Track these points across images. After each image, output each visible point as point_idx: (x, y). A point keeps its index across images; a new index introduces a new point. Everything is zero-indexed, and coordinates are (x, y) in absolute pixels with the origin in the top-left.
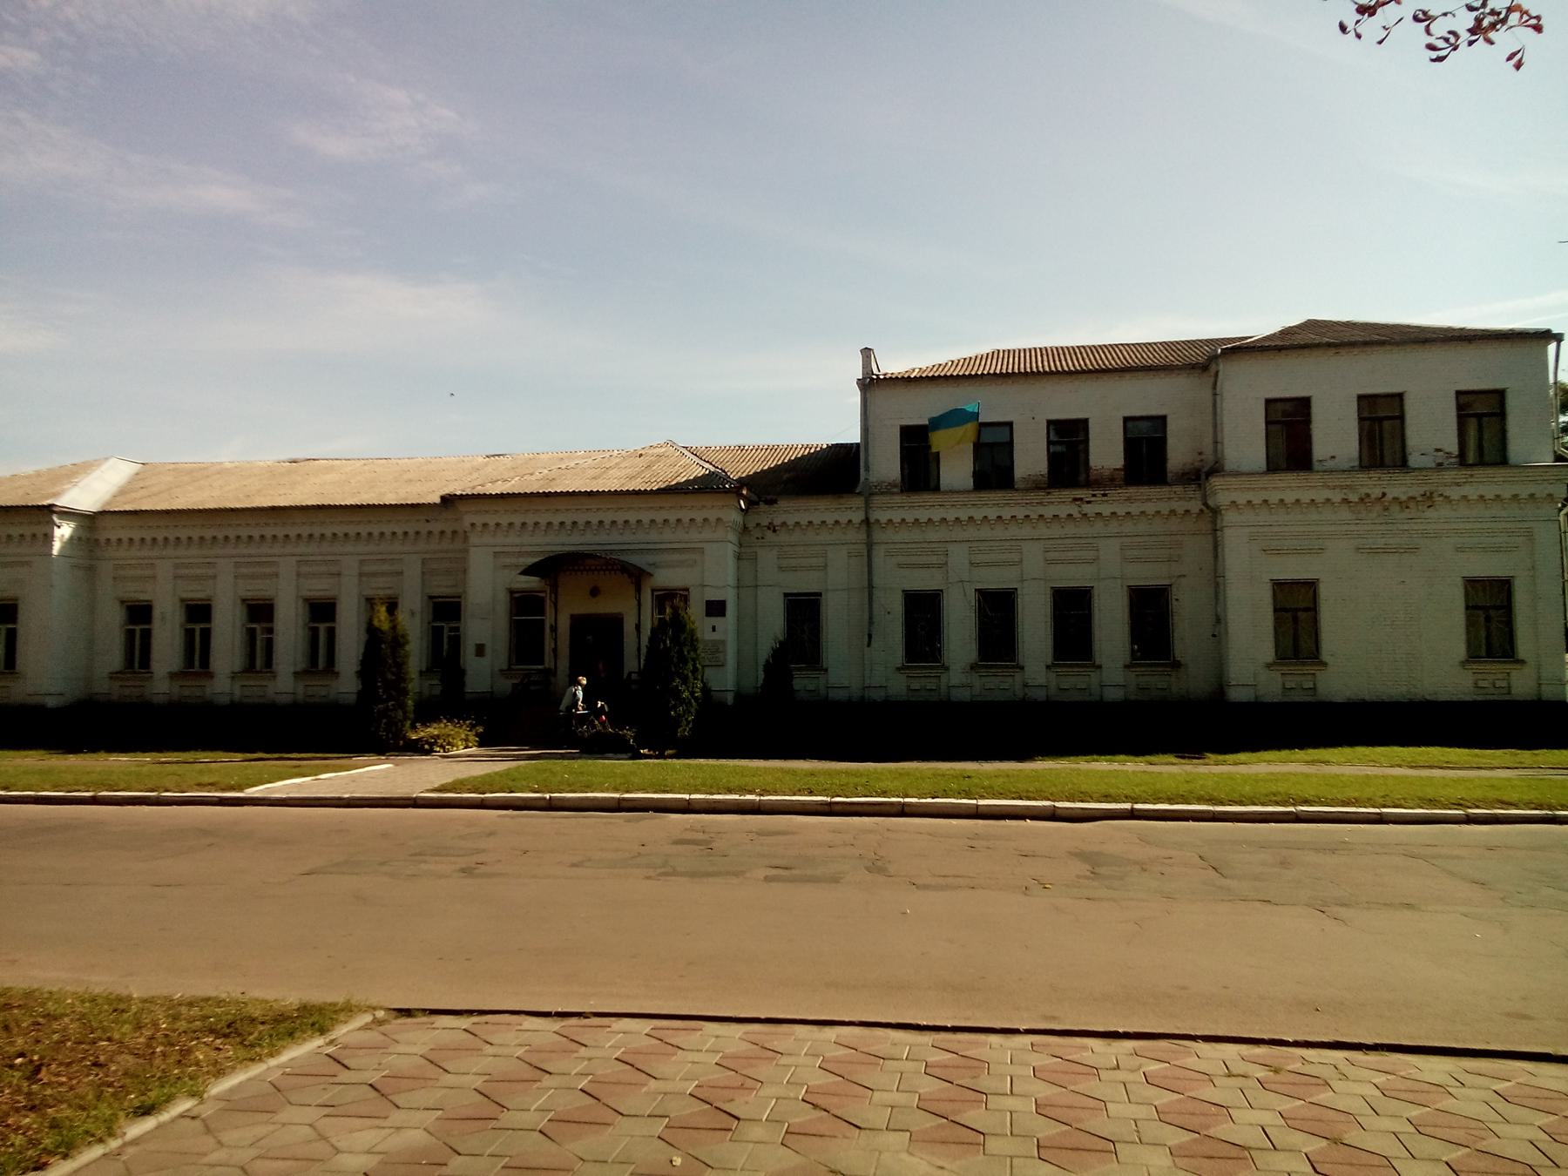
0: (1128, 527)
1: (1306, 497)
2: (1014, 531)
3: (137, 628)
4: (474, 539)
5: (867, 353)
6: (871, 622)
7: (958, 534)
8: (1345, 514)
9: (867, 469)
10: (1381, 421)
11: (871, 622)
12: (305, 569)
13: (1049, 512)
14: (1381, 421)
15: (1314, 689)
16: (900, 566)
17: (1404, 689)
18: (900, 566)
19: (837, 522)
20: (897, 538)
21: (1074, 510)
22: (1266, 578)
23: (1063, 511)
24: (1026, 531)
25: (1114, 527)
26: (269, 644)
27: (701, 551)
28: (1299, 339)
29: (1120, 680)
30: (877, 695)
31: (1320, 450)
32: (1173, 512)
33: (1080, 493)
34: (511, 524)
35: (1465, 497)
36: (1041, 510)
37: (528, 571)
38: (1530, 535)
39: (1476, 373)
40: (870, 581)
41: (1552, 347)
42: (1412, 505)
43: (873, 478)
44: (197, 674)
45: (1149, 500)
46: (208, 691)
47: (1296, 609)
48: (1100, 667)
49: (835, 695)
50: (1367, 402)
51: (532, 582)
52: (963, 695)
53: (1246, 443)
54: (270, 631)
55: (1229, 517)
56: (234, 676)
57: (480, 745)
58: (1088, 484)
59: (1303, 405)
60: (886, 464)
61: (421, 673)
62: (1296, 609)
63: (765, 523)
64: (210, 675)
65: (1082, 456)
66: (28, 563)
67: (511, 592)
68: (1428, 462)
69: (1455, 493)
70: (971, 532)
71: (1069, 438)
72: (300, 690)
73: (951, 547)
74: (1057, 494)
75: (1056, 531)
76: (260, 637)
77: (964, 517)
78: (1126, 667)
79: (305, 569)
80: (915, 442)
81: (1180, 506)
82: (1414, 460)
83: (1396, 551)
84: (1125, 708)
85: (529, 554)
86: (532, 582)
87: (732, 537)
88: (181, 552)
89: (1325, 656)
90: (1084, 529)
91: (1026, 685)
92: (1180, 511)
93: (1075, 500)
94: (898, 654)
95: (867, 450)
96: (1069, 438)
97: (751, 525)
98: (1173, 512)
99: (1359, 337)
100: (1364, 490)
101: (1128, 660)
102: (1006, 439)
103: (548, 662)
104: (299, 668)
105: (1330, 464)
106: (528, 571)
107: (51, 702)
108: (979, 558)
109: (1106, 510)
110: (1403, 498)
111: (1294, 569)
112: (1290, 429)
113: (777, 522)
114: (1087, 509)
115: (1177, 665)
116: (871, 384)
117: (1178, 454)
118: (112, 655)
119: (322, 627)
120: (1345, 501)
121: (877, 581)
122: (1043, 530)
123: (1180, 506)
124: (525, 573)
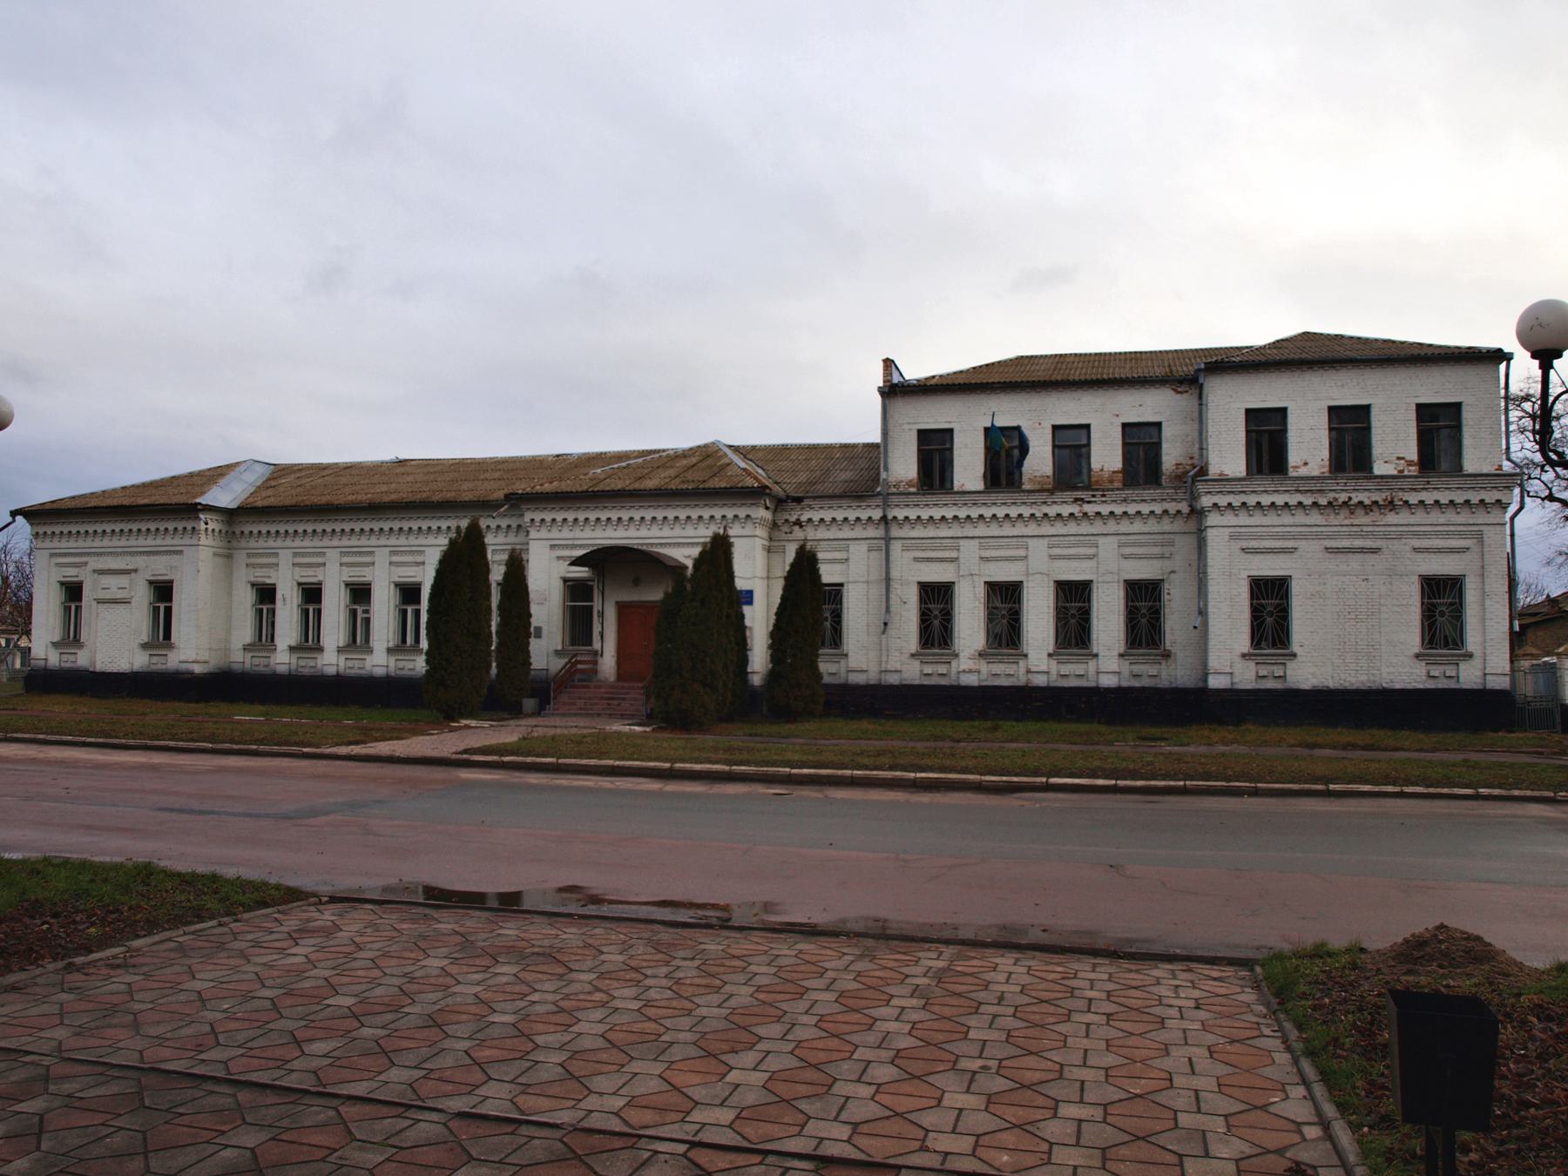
0: (1125, 526)
1: (1280, 500)
2: (1020, 529)
3: (265, 608)
4: (533, 534)
5: (889, 364)
6: (888, 610)
7: (969, 530)
8: (1315, 518)
9: (886, 469)
10: (1350, 431)
11: (888, 610)
12: (395, 559)
13: (1052, 511)
14: (1350, 431)
15: (1283, 677)
16: (916, 559)
17: (1363, 678)
18: (916, 559)
19: (858, 519)
20: (914, 534)
21: (1075, 509)
22: (1244, 574)
23: (1065, 510)
24: (1032, 529)
25: (1112, 526)
26: (367, 621)
27: (276, 555)
28: (1285, 355)
29: (1115, 667)
30: (893, 679)
31: (1294, 458)
32: (1166, 512)
33: (1079, 494)
34: (543, 520)
35: (1422, 502)
36: (1045, 509)
37: (577, 562)
38: (1480, 538)
39: (1436, 387)
40: (888, 573)
41: (1503, 366)
42: (1375, 508)
43: (892, 479)
44: (310, 649)
45: (1146, 503)
46: (272, 661)
47: (1270, 606)
48: (1096, 655)
49: (855, 679)
50: (924, 436)
51: (581, 572)
52: (971, 680)
53: (1228, 454)
54: (367, 612)
55: (1212, 519)
56: (340, 650)
57: (648, 719)
58: (1088, 488)
59: (1280, 414)
60: (904, 466)
61: (389, 650)
62: (1270, 606)
63: (793, 519)
64: (320, 649)
65: (1084, 464)
66: (181, 552)
67: (565, 580)
68: (1390, 470)
69: (1413, 498)
70: (981, 530)
71: (1072, 444)
72: (392, 664)
73: (962, 542)
74: (1058, 496)
75: (1059, 528)
76: (360, 616)
77: (1158, 510)
78: (1121, 655)
79: (395, 559)
80: (935, 451)
81: (1172, 507)
82: (1379, 468)
83: (1362, 550)
84: (1119, 692)
85: (581, 546)
86: (581, 572)
87: (761, 532)
88: (298, 543)
89: (1295, 648)
90: (1085, 528)
91: (1029, 672)
92: (1172, 512)
93: (1076, 500)
94: (913, 643)
95: (886, 451)
96: (1072, 444)
97: (779, 523)
98: (1166, 512)
99: (1368, 353)
100: (1331, 495)
101: (1051, 649)
102: (1084, 442)
103: (597, 645)
104: (56, 638)
105: (1303, 471)
106: (577, 562)
107: (198, 669)
108: (987, 554)
109: (1105, 509)
110: (1367, 502)
111: (1269, 567)
112: (1267, 437)
113: (804, 518)
114: (1088, 508)
115: (1167, 655)
116: (895, 390)
117: (1172, 455)
118: (244, 632)
119: (410, 609)
120: (1315, 504)
121: (894, 574)
122: (1046, 529)
123: (1172, 507)
124: (572, 564)
